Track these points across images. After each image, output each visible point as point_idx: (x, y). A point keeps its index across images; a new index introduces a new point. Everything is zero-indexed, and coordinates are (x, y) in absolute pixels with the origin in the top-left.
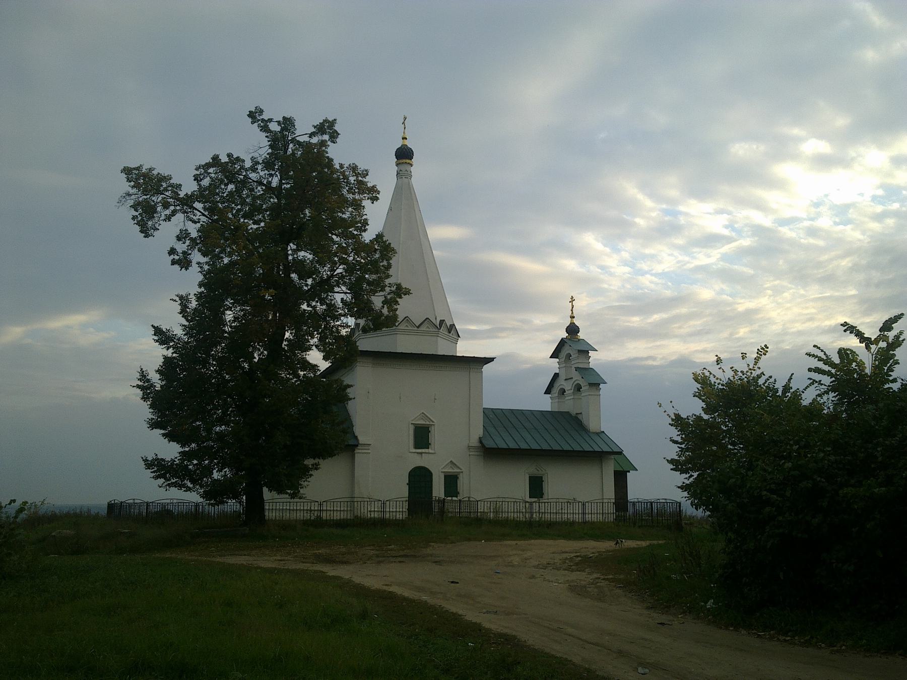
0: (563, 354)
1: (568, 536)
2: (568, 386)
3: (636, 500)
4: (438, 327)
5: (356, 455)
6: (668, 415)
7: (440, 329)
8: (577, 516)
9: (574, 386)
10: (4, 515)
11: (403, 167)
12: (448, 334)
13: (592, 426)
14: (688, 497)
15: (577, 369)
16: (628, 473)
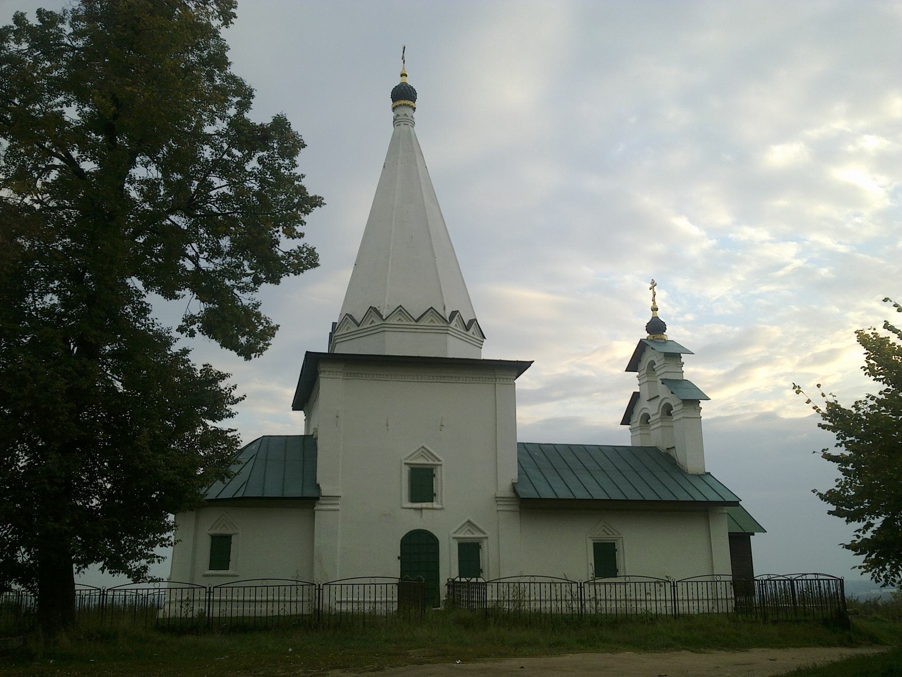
0: (644, 364)
1: (642, 645)
2: (653, 409)
3: (765, 577)
4: (448, 321)
5: (317, 512)
6: (814, 408)
7: (450, 323)
8: (663, 604)
9: (661, 408)
11: (401, 111)
12: (464, 332)
13: (691, 467)
14: (864, 567)
15: (664, 381)
16: (751, 537)
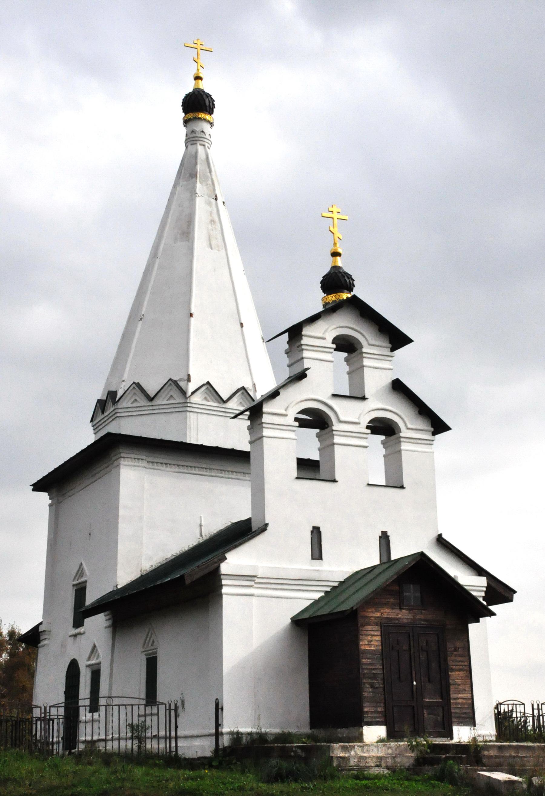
10: (2, 777)
